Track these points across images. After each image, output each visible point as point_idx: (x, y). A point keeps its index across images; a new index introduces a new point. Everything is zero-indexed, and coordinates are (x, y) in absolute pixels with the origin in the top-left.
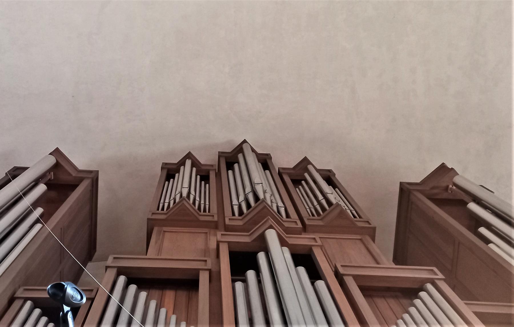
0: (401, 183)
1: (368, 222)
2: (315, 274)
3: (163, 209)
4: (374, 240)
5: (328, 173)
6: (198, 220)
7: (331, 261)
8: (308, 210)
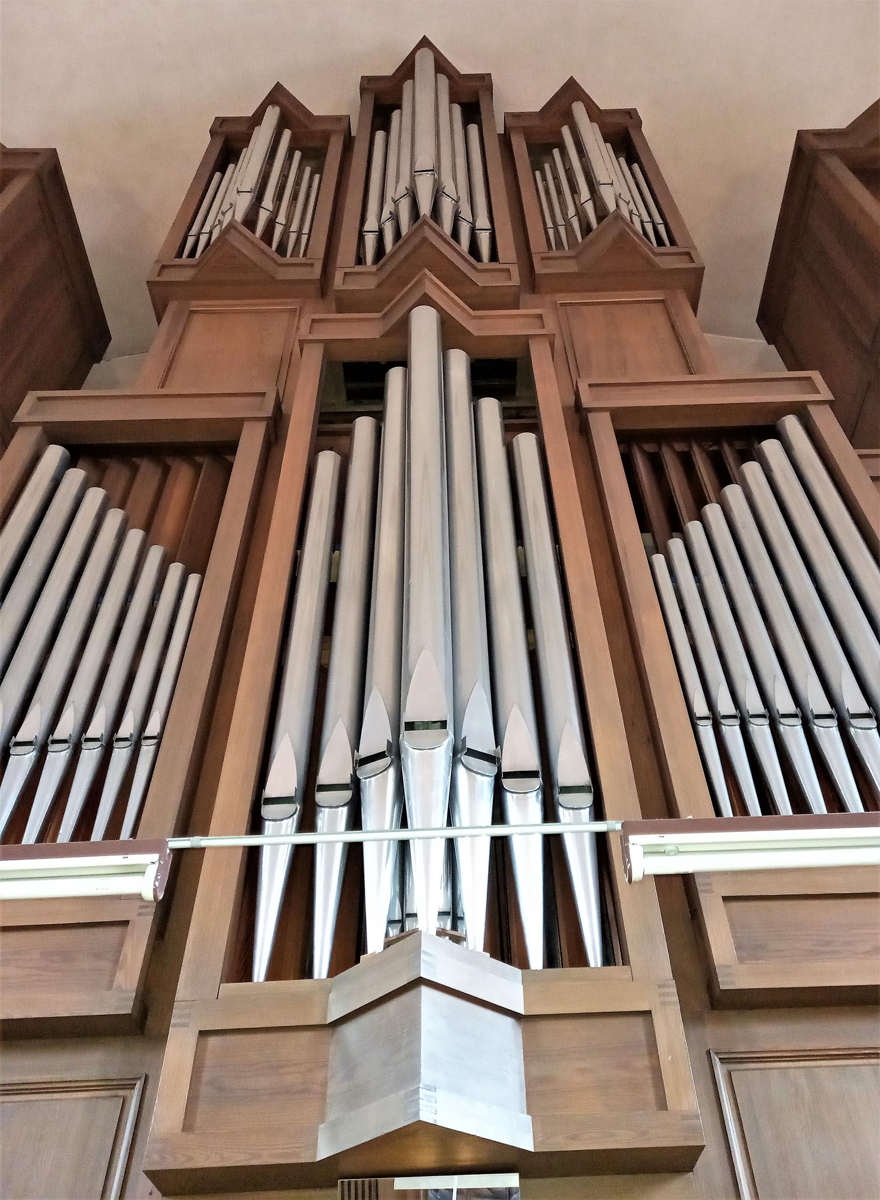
0: (800, 134)
1: (688, 254)
2: (521, 418)
3: (192, 254)
4: (695, 309)
5: (626, 121)
6: (273, 280)
7: (88, 1081)
8: (551, 232)
